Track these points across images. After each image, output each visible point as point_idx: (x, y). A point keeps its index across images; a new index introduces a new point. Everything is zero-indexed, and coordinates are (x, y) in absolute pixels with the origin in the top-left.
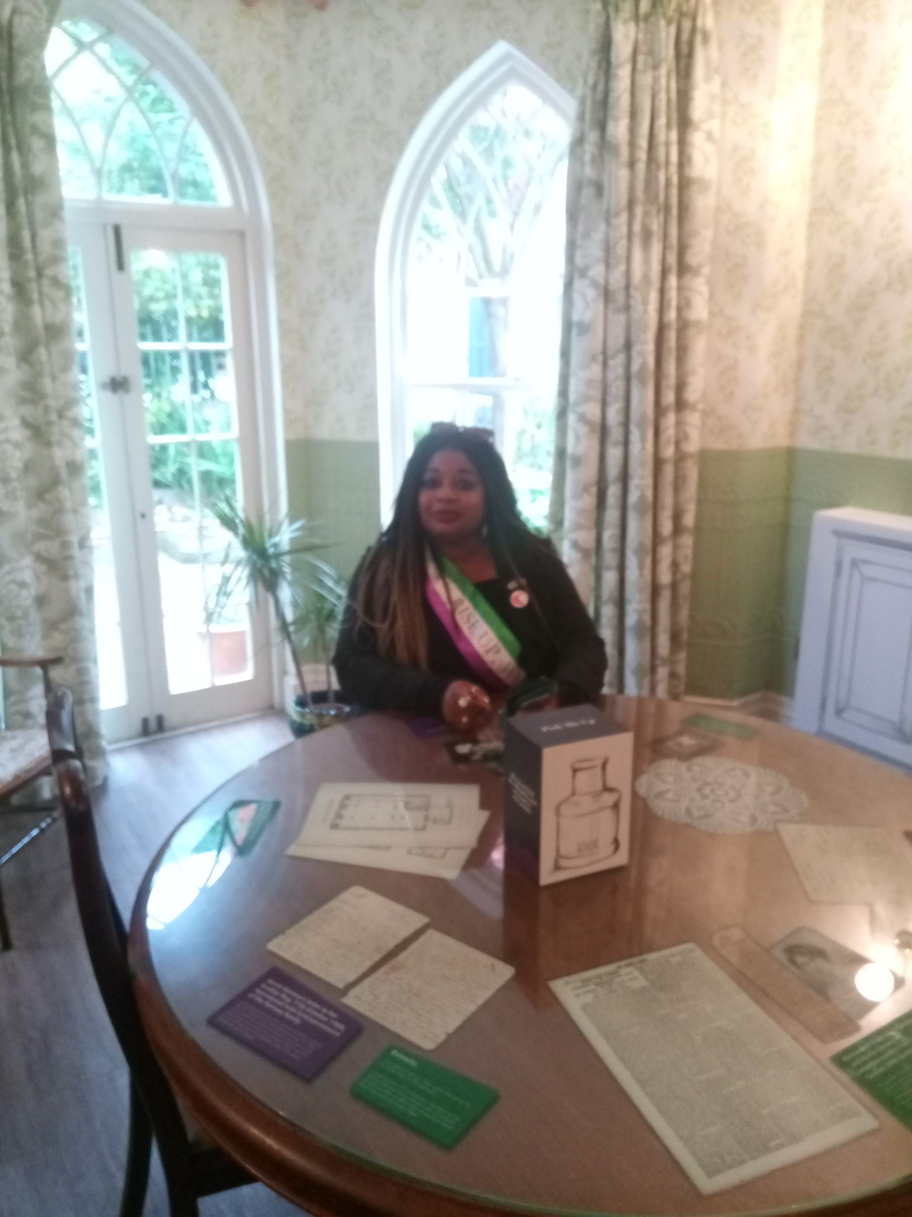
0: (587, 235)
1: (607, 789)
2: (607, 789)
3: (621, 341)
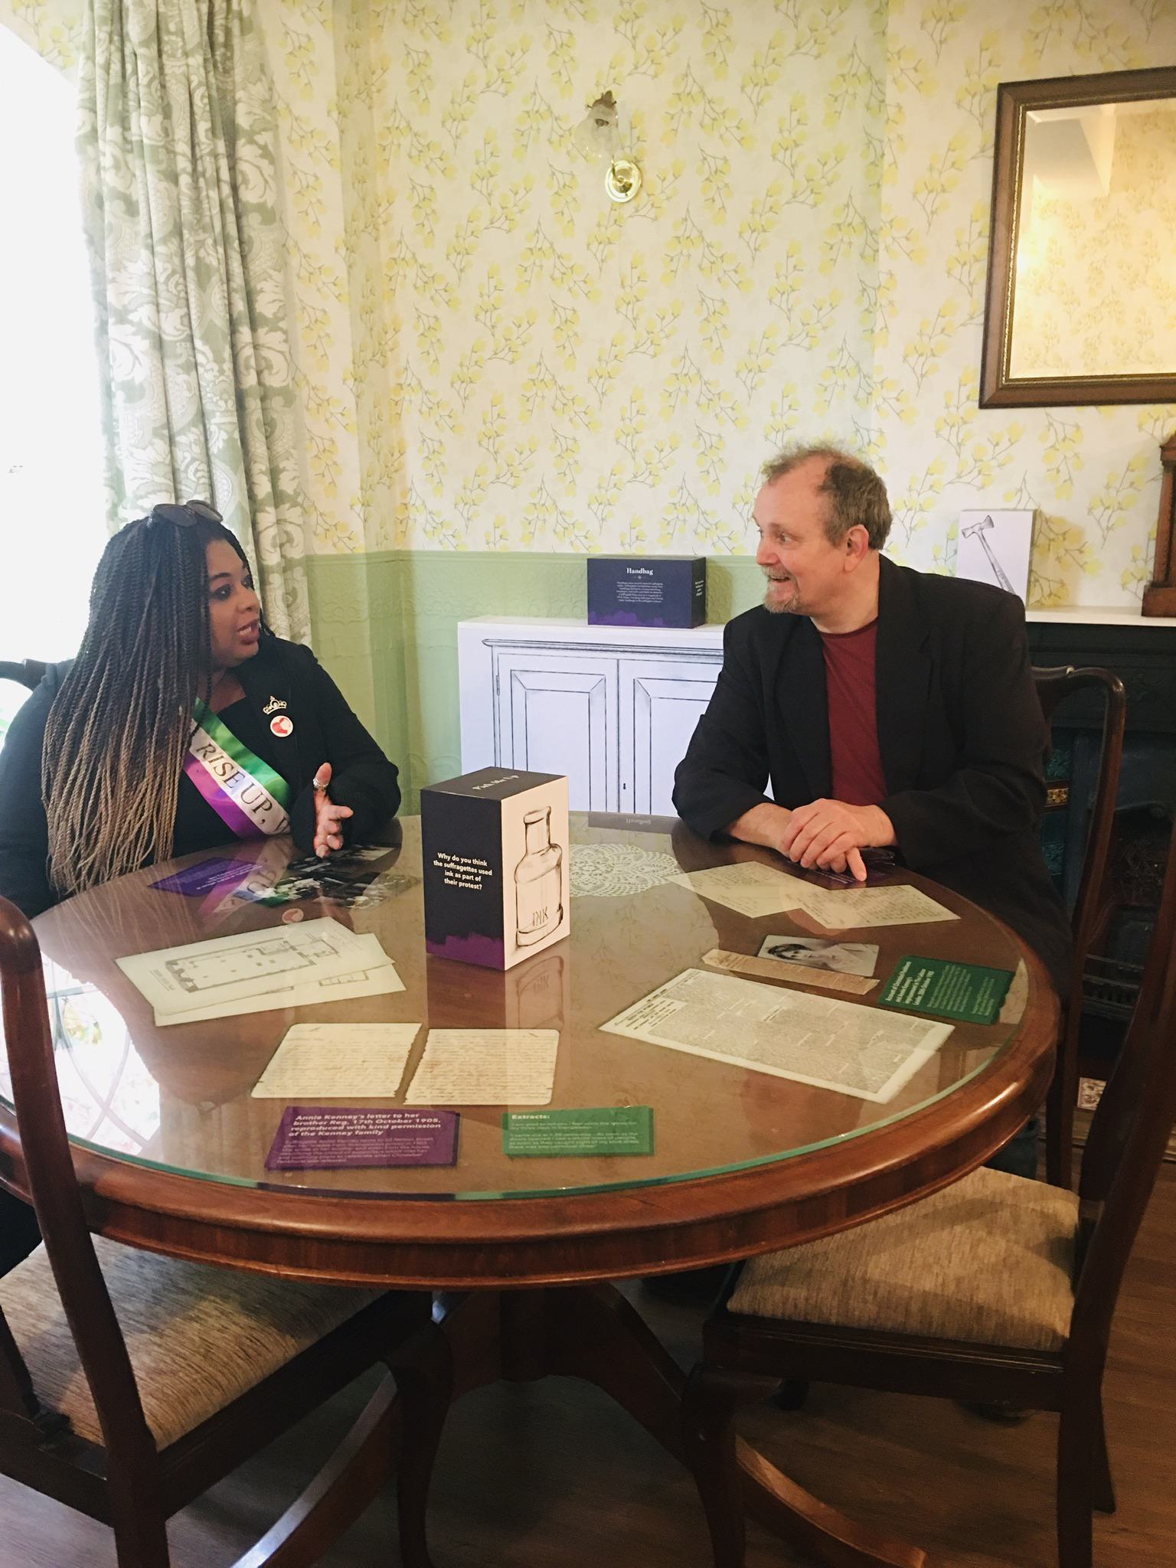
0: (119, 266)
1: (552, 846)
2: (552, 846)
3: (192, 411)
